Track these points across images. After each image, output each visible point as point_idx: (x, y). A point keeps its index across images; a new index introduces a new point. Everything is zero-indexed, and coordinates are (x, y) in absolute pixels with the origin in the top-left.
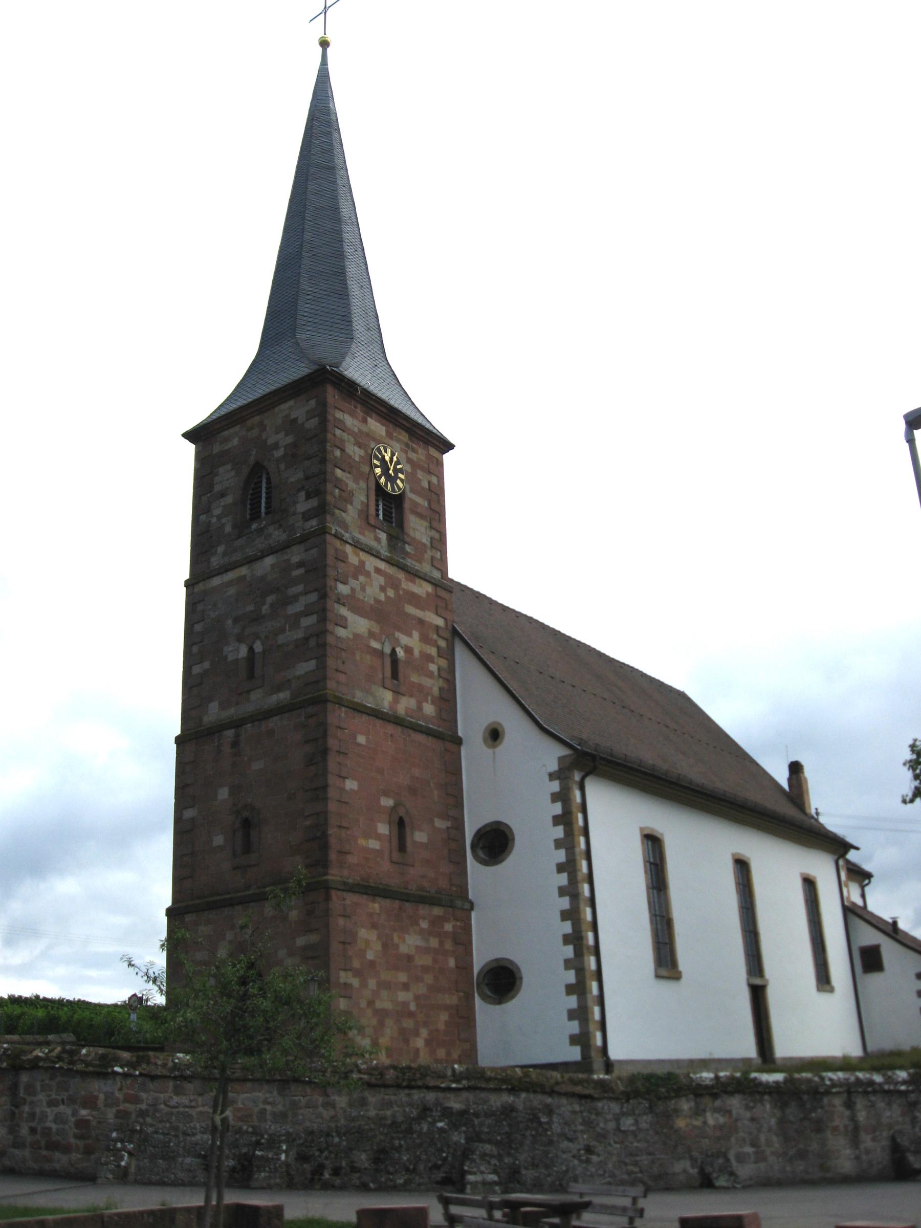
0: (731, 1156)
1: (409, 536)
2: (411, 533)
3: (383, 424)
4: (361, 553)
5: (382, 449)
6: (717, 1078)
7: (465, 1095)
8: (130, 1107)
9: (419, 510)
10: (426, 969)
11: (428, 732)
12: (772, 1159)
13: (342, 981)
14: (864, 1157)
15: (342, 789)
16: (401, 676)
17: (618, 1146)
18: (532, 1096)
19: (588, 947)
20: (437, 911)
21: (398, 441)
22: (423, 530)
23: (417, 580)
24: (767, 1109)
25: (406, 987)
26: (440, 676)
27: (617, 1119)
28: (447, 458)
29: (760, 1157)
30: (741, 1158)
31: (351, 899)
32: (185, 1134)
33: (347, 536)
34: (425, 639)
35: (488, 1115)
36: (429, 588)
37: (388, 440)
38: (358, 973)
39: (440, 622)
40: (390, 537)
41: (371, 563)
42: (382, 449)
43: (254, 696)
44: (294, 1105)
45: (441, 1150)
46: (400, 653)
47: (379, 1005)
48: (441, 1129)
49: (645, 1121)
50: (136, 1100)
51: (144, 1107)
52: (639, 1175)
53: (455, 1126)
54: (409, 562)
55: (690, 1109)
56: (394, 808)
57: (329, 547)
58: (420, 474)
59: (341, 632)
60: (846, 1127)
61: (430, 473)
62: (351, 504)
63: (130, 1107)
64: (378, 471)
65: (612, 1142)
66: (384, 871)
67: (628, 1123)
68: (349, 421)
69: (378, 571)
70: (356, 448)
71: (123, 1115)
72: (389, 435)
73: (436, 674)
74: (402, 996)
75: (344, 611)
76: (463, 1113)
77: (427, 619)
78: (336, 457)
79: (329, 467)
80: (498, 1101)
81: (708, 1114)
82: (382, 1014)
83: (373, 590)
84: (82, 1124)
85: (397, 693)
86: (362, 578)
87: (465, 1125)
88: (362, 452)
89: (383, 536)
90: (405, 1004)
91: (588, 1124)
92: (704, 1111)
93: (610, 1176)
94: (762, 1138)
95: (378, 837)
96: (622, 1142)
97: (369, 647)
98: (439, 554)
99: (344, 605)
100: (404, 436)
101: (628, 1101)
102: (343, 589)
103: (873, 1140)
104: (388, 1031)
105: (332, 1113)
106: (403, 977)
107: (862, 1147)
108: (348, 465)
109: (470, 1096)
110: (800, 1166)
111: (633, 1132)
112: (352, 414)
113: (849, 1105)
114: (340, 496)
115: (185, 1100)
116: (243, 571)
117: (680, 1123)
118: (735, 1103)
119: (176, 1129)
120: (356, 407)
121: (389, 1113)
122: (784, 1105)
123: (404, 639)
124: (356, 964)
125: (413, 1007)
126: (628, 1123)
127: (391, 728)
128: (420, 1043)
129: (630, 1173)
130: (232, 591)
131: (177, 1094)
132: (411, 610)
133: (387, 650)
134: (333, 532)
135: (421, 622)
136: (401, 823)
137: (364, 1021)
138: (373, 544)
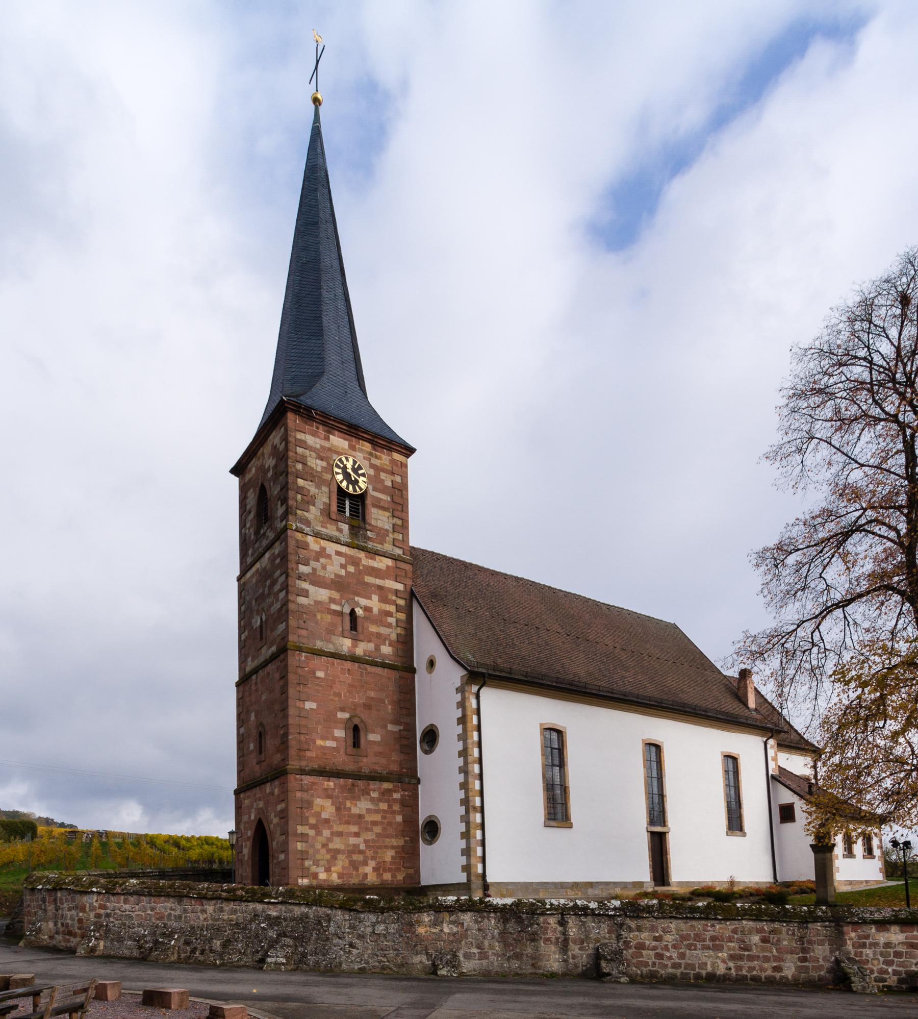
0: (460, 955)
1: (370, 525)
2: (373, 522)
3: (345, 439)
4: (322, 541)
5: (344, 459)
6: (458, 900)
7: (279, 907)
8: (102, 911)
9: (382, 504)
10: (374, 823)
11: (383, 665)
13: (299, 831)
14: (571, 961)
15: (302, 709)
16: (359, 628)
18: (319, 909)
19: (475, 808)
20: (386, 785)
21: (361, 451)
22: (385, 519)
23: (377, 558)
24: (492, 923)
25: (357, 835)
26: (397, 626)
27: (374, 925)
28: (412, 461)
31: (307, 779)
32: (129, 927)
33: (307, 530)
34: (384, 600)
35: (293, 919)
36: (390, 562)
37: (350, 452)
38: (312, 827)
39: (400, 587)
40: (352, 528)
41: (331, 548)
42: (344, 459)
43: (264, 650)
44: (185, 911)
45: (261, 942)
46: (359, 612)
47: (331, 846)
48: (263, 928)
50: (105, 907)
51: (109, 911)
53: (271, 926)
54: (370, 545)
55: (430, 921)
56: (350, 719)
57: (290, 539)
58: (383, 476)
59: (302, 600)
61: (393, 474)
62: (314, 505)
63: (102, 911)
64: (340, 477)
66: (341, 760)
67: (380, 928)
68: (310, 440)
69: (338, 553)
70: (319, 462)
71: (98, 916)
72: (352, 447)
73: (394, 624)
74: (353, 840)
75: (305, 585)
76: (278, 918)
77: (387, 586)
78: (297, 470)
79: (291, 479)
80: (298, 911)
82: (335, 853)
83: (334, 568)
84: (80, 921)
85: (355, 640)
86: (322, 560)
87: (277, 925)
88: (324, 464)
89: (345, 527)
90: (356, 846)
91: (353, 927)
92: (442, 922)
94: (486, 943)
95: (335, 739)
96: (376, 941)
97: (329, 609)
98: (401, 536)
99: (305, 580)
100: (367, 447)
101: (382, 913)
102: (303, 569)
103: (580, 949)
105: (205, 916)
106: (354, 829)
108: (310, 475)
109: (283, 908)
111: (384, 935)
112: (314, 434)
113: (562, 923)
114: (302, 500)
115: (127, 907)
116: (258, 566)
117: (421, 930)
118: (467, 918)
119: (125, 924)
120: (318, 428)
121: (234, 917)
122: (506, 921)
123: (363, 602)
124: (312, 821)
126: (380, 928)
127: (348, 665)
128: (368, 869)
129: (380, 962)
130: (254, 580)
131: (125, 903)
132: (369, 579)
133: (347, 610)
134: (294, 527)
135: (380, 588)
136: (356, 729)
137: (318, 857)
138: (337, 534)
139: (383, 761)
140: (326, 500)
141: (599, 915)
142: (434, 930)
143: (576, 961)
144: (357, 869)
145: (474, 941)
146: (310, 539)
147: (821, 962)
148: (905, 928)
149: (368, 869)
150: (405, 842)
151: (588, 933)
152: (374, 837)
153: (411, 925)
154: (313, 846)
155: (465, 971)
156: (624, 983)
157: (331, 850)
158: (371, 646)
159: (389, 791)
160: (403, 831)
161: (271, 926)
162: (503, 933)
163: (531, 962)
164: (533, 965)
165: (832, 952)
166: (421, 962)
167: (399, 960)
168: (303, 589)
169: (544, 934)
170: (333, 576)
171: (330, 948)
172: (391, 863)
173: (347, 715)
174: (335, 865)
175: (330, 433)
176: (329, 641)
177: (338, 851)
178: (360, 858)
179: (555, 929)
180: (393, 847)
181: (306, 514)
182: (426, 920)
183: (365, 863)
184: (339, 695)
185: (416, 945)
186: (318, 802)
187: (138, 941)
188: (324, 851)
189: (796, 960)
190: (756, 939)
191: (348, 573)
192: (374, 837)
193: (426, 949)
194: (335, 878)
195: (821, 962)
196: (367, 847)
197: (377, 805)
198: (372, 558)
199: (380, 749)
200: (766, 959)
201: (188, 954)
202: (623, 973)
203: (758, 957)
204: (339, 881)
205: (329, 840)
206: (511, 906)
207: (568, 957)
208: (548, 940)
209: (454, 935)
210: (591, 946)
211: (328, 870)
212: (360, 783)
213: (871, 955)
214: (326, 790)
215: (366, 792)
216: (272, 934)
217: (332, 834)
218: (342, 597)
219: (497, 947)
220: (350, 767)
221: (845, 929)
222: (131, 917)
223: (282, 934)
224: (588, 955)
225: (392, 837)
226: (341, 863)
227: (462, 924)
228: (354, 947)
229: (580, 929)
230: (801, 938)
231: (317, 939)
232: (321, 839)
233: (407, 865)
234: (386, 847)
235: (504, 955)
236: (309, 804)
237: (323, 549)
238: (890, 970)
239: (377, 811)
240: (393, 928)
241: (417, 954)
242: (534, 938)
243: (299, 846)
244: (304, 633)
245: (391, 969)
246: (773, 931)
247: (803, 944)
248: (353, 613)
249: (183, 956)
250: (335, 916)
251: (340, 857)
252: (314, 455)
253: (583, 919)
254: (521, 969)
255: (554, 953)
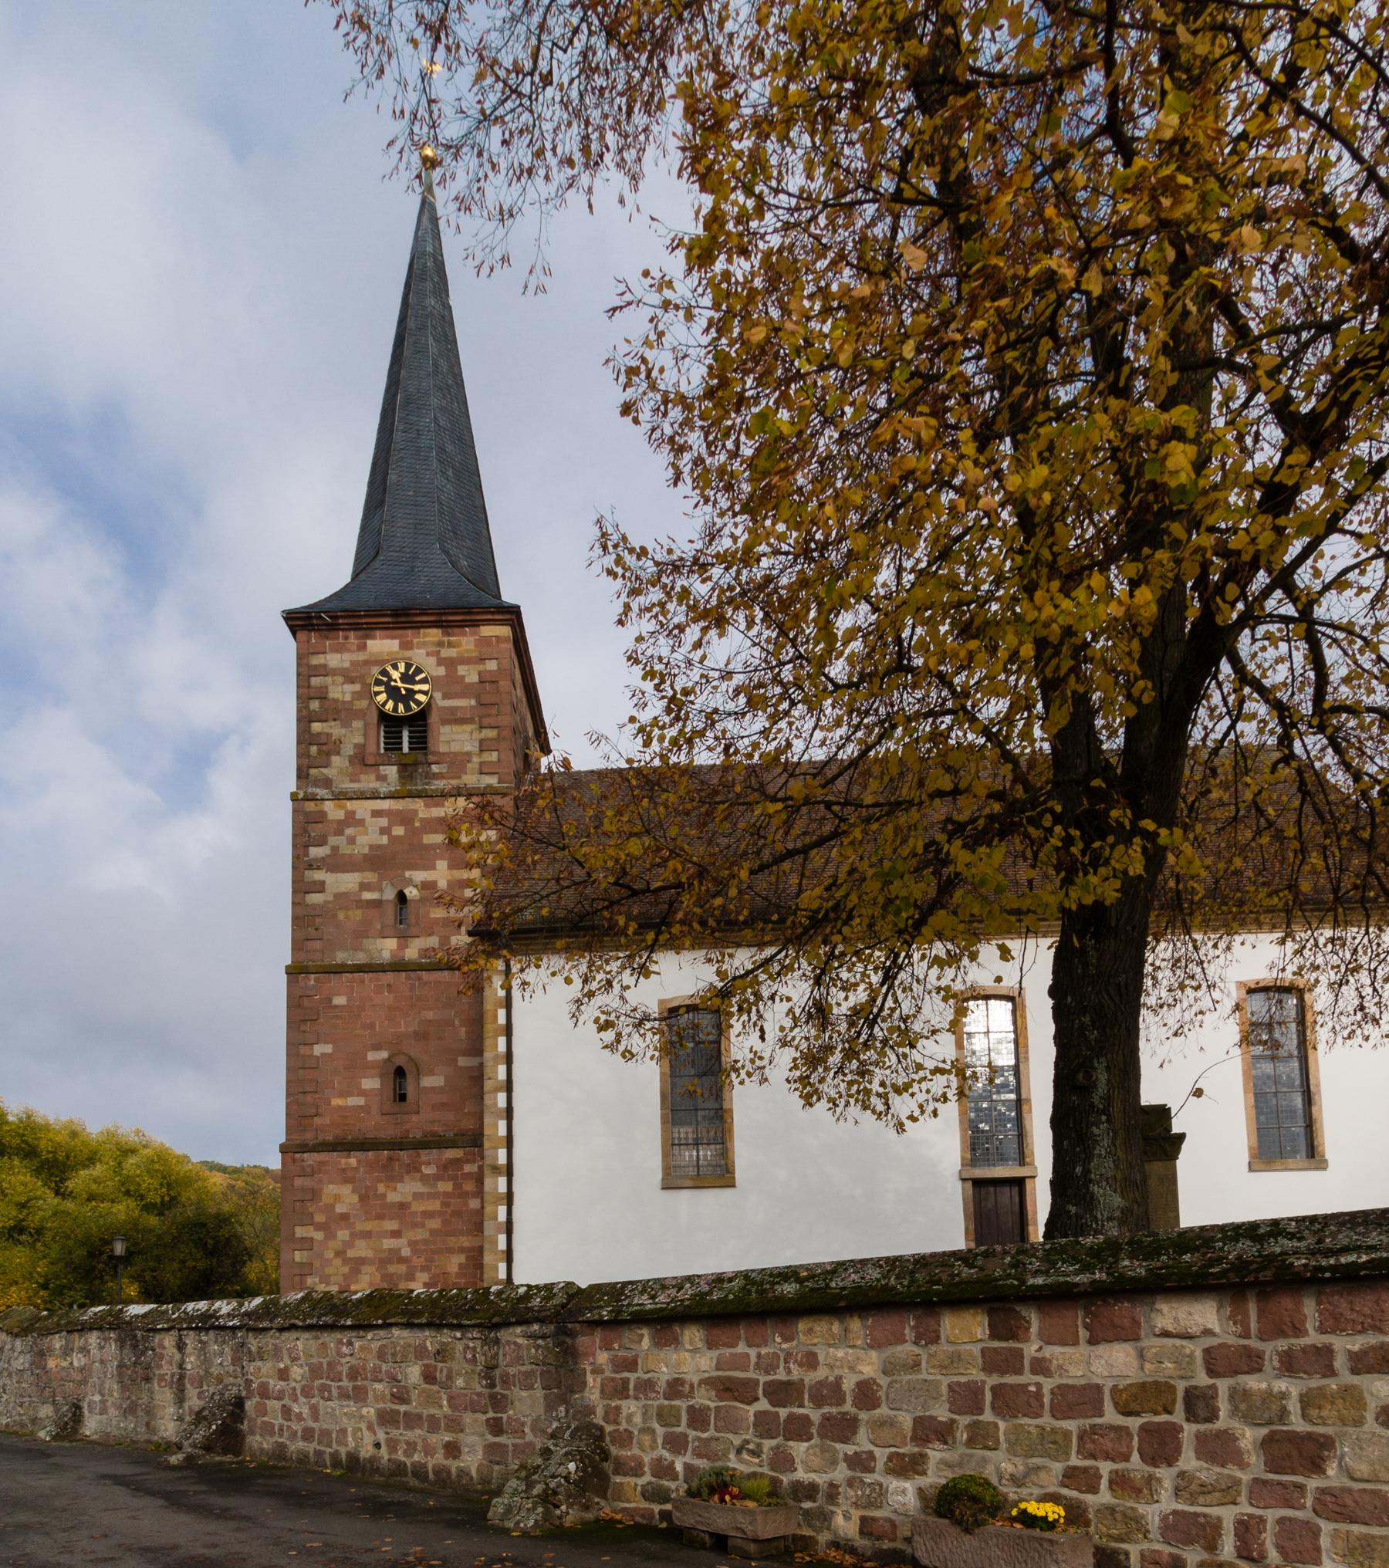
1: (435, 753)
20: (450, 1154)
21: (422, 645)
22: (467, 736)
25: (396, 1234)
33: (321, 792)
38: (319, 1227)
46: (411, 893)
47: (350, 1254)
66: (375, 1125)
69: (376, 814)
74: (388, 1243)
85: (404, 938)
88: (357, 687)
95: (362, 1093)
106: (391, 1225)
112: (339, 649)
114: (319, 752)
123: (419, 876)
124: (320, 1218)
127: (389, 977)
133: (390, 894)
137: (329, 1270)
139: (450, 1116)
140: (359, 739)
146: (328, 806)
147: (530, 1437)
148: (722, 1333)
152: (427, 1235)
158: (433, 941)
159: (457, 1163)
165: (550, 1407)
168: (315, 882)
170: (366, 851)
172: (457, 1275)
173: (385, 1055)
175: (368, 637)
176: (357, 948)
177: (362, 1261)
178: (402, 1269)
180: (462, 1250)
181: (324, 771)
183: (411, 1277)
184: (372, 1026)
186: (330, 1189)
189: (483, 1429)
190: (414, 1373)
191: (393, 840)
192: (427, 1235)
195: (530, 1437)
196: (414, 1251)
197: (434, 1186)
198: (437, 805)
199: (444, 1098)
200: (433, 1425)
203: (419, 1417)
205: (349, 1244)
212: (404, 1155)
213: (638, 1419)
214: (344, 1170)
215: (414, 1168)
217: (353, 1235)
218: (381, 879)
220: (389, 1132)
221: (583, 1341)
230: (490, 1368)
234: (450, 1251)
236: (315, 1194)
237: (351, 814)
238: (679, 1467)
239: (431, 1196)
243: (298, 1256)
244: (317, 945)
246: (442, 1354)
247: (492, 1386)
248: (402, 898)
251: (366, 1269)
252: (340, 679)
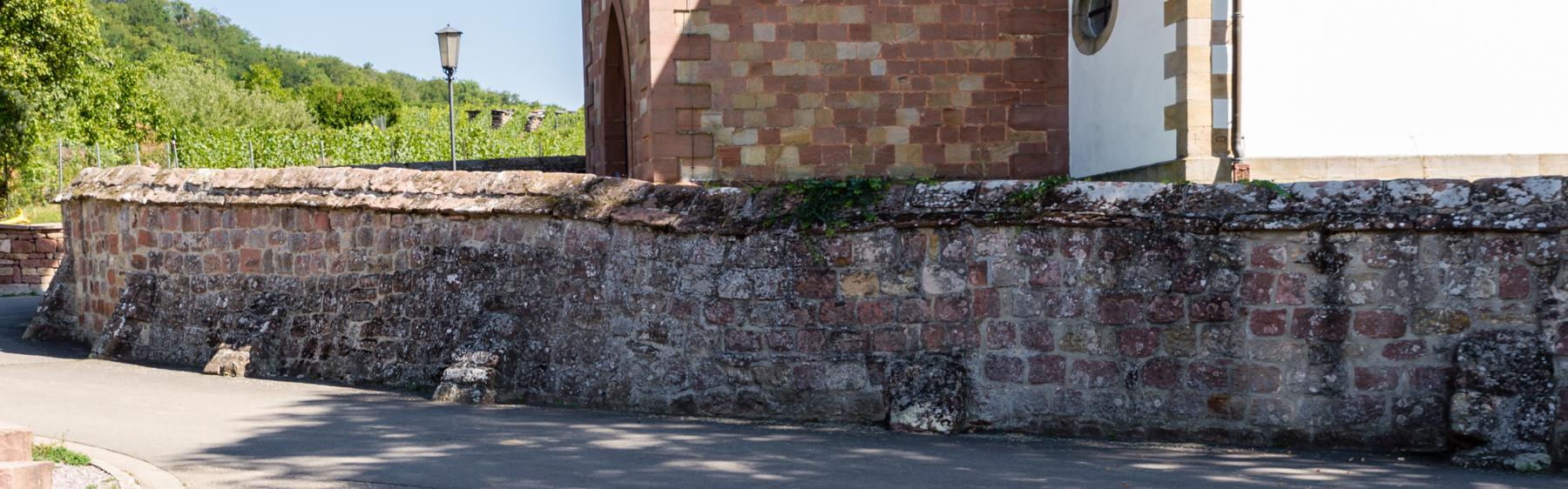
0: (975, 365)
12: (1074, 378)
14: (1352, 391)
17: (715, 328)
25: (860, 33)
27: (716, 273)
29: (1047, 369)
30: (997, 370)
35: (522, 260)
45: (446, 325)
47: (779, 68)
48: (451, 286)
49: (771, 279)
52: (754, 389)
53: (469, 280)
60: (1303, 316)
65: (702, 319)
74: (846, 50)
76: (487, 256)
81: (926, 271)
90: (858, 67)
92: (918, 263)
93: (693, 387)
94: (1058, 329)
96: (723, 322)
101: (741, 237)
103: (1389, 352)
104: (807, 118)
107: (1349, 367)
110: (1153, 399)
113: (1327, 261)
115: (188, 238)
117: (851, 288)
118: (997, 246)
125: (878, 68)
128: (897, 135)
137: (739, 100)
141: (1467, 230)
142: (895, 289)
143: (1372, 393)
144: (861, 135)
145: (1017, 322)
149: (897, 135)
150: (1020, 46)
151: (1420, 295)
153: (822, 272)
154: (724, 72)
155: (986, 416)
156: (1527, 472)
157: (781, 79)
160: (1011, 15)
161: (469, 280)
162: (1113, 302)
163: (1207, 393)
164: (1214, 404)
166: (850, 386)
167: (787, 379)
169: (1254, 299)
171: (603, 343)
172: (972, 114)
174: (791, 125)
177: (798, 84)
178: (873, 100)
179: (1298, 283)
180: (977, 67)
182: (869, 255)
185: (836, 335)
187: (211, 324)
188: (756, 84)
193: (868, 345)
194: (790, 161)
196: (891, 66)
201: (299, 358)
202: (1534, 438)
204: (807, 172)
205: (774, 51)
206: (1146, 206)
207: (1342, 378)
208: (1271, 318)
209: (956, 301)
210: (1432, 341)
211: (770, 139)
216: (472, 302)
217: (781, 32)
219: (1095, 342)
222: (195, 263)
223: (494, 304)
224: (1419, 376)
225: (975, 34)
226: (810, 117)
227: (983, 268)
228: (663, 339)
229: (1390, 281)
231: (573, 316)
232: (749, 50)
233: (1025, 118)
234: (956, 66)
235: (1114, 368)
240: (771, 279)
241: (839, 361)
242: (1216, 313)
245: (766, 406)
249: (290, 361)
250: (618, 247)
251: (806, 99)
253: (1404, 245)
254: (1172, 415)
255: (1292, 365)
